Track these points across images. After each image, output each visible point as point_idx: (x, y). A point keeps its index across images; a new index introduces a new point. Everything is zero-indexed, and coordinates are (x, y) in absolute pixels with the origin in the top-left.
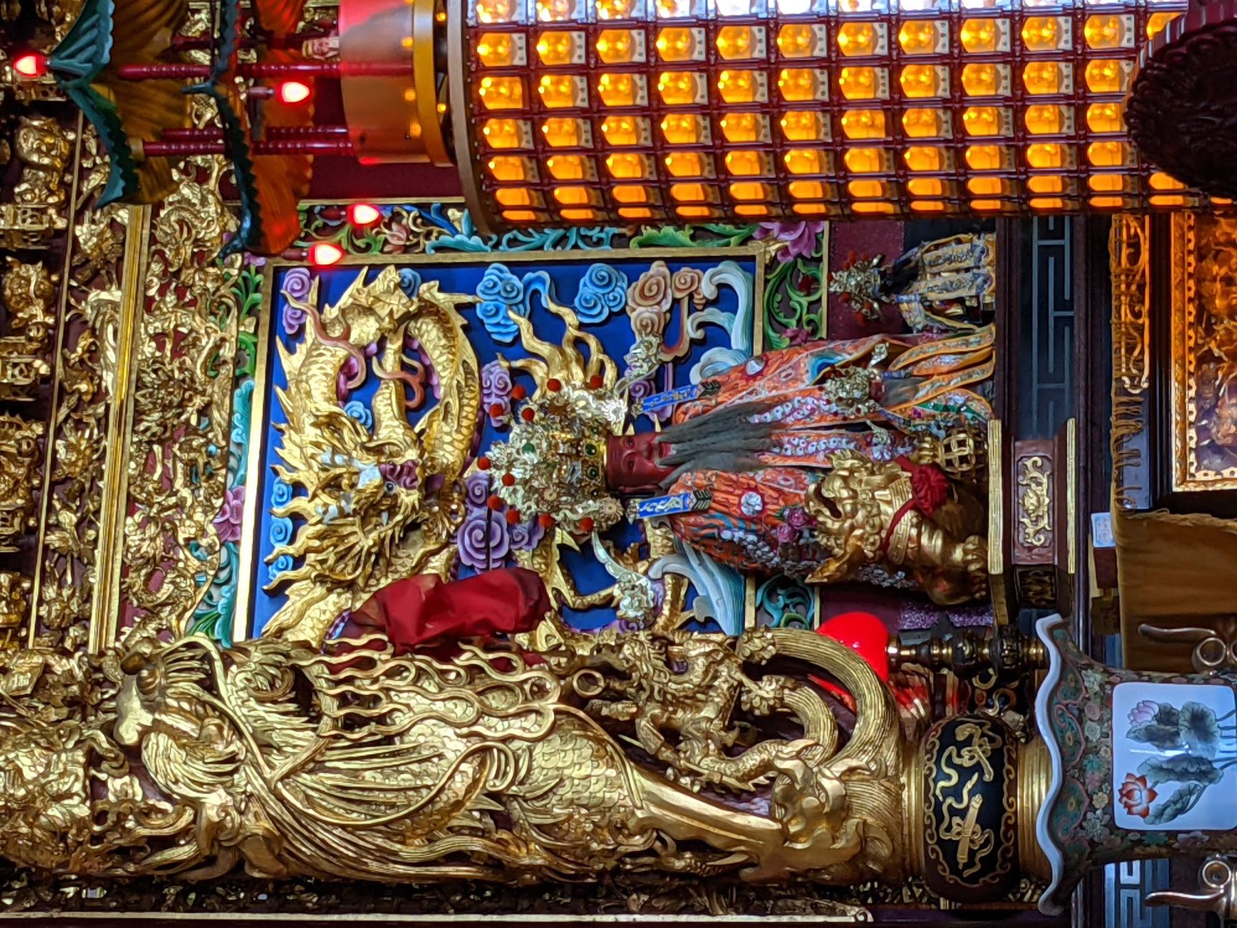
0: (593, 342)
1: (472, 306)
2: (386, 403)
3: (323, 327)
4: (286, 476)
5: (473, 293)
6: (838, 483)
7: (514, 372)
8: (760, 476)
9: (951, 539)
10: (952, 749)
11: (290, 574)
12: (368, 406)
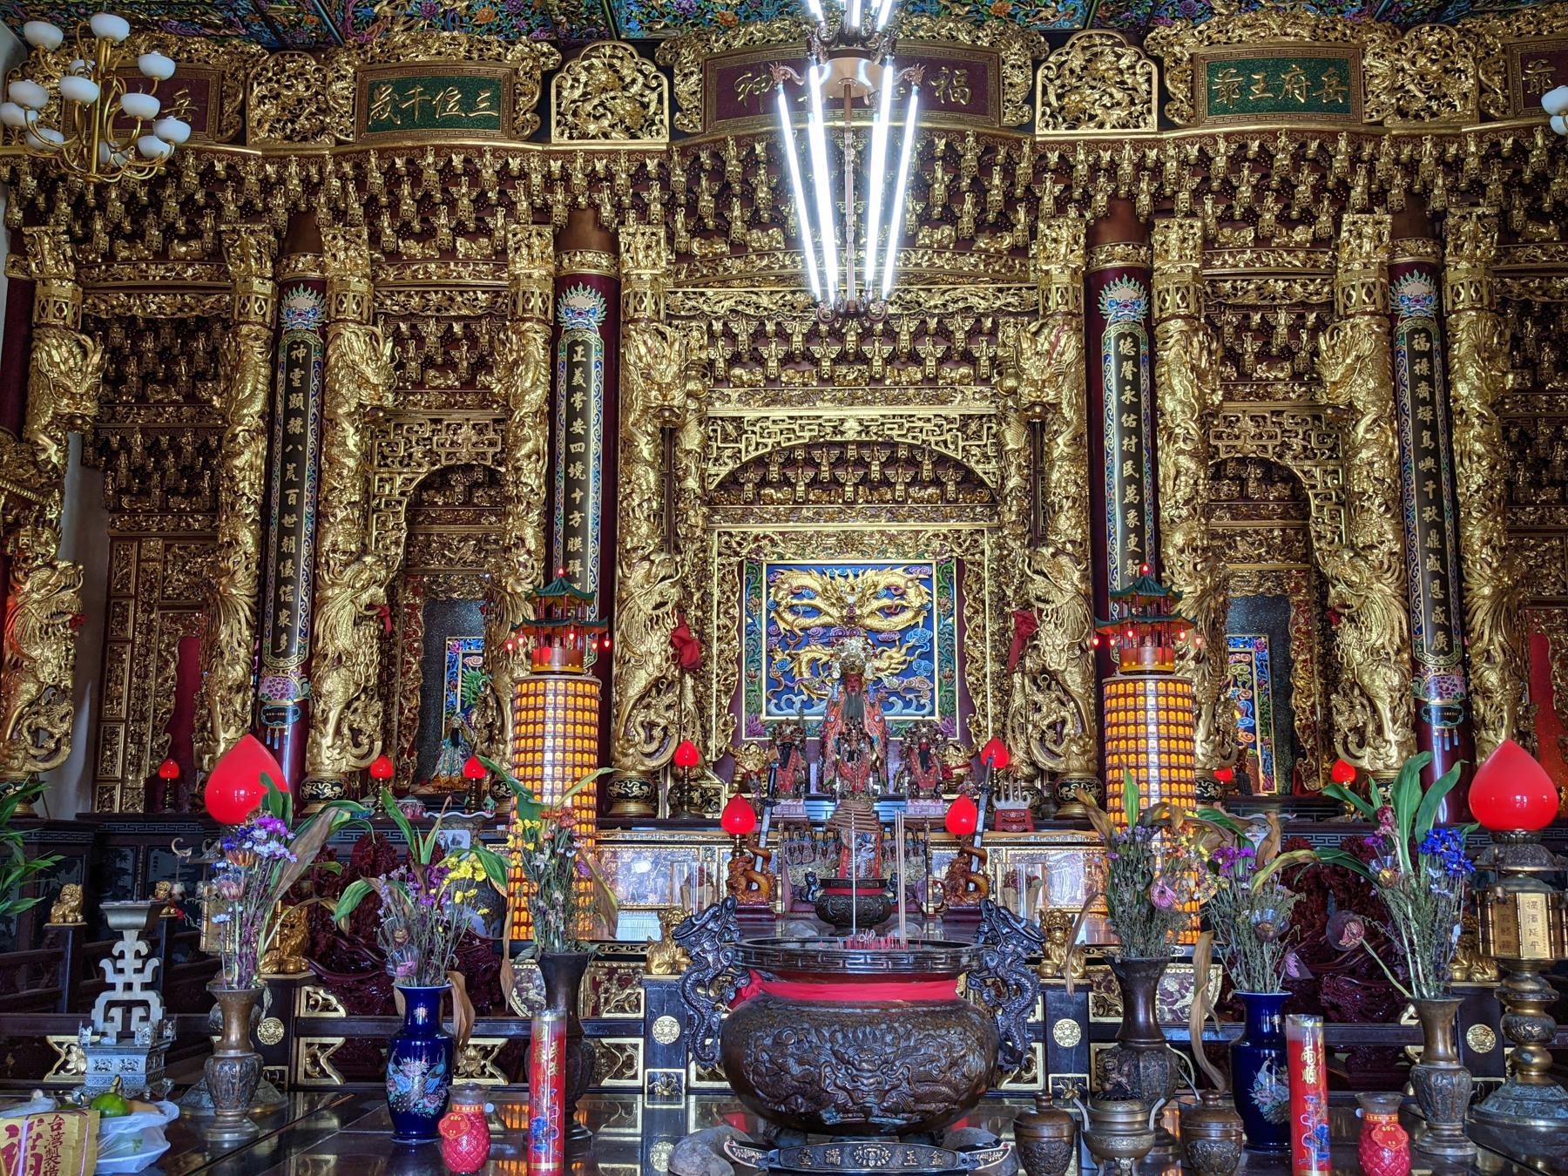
2: (886, 602)
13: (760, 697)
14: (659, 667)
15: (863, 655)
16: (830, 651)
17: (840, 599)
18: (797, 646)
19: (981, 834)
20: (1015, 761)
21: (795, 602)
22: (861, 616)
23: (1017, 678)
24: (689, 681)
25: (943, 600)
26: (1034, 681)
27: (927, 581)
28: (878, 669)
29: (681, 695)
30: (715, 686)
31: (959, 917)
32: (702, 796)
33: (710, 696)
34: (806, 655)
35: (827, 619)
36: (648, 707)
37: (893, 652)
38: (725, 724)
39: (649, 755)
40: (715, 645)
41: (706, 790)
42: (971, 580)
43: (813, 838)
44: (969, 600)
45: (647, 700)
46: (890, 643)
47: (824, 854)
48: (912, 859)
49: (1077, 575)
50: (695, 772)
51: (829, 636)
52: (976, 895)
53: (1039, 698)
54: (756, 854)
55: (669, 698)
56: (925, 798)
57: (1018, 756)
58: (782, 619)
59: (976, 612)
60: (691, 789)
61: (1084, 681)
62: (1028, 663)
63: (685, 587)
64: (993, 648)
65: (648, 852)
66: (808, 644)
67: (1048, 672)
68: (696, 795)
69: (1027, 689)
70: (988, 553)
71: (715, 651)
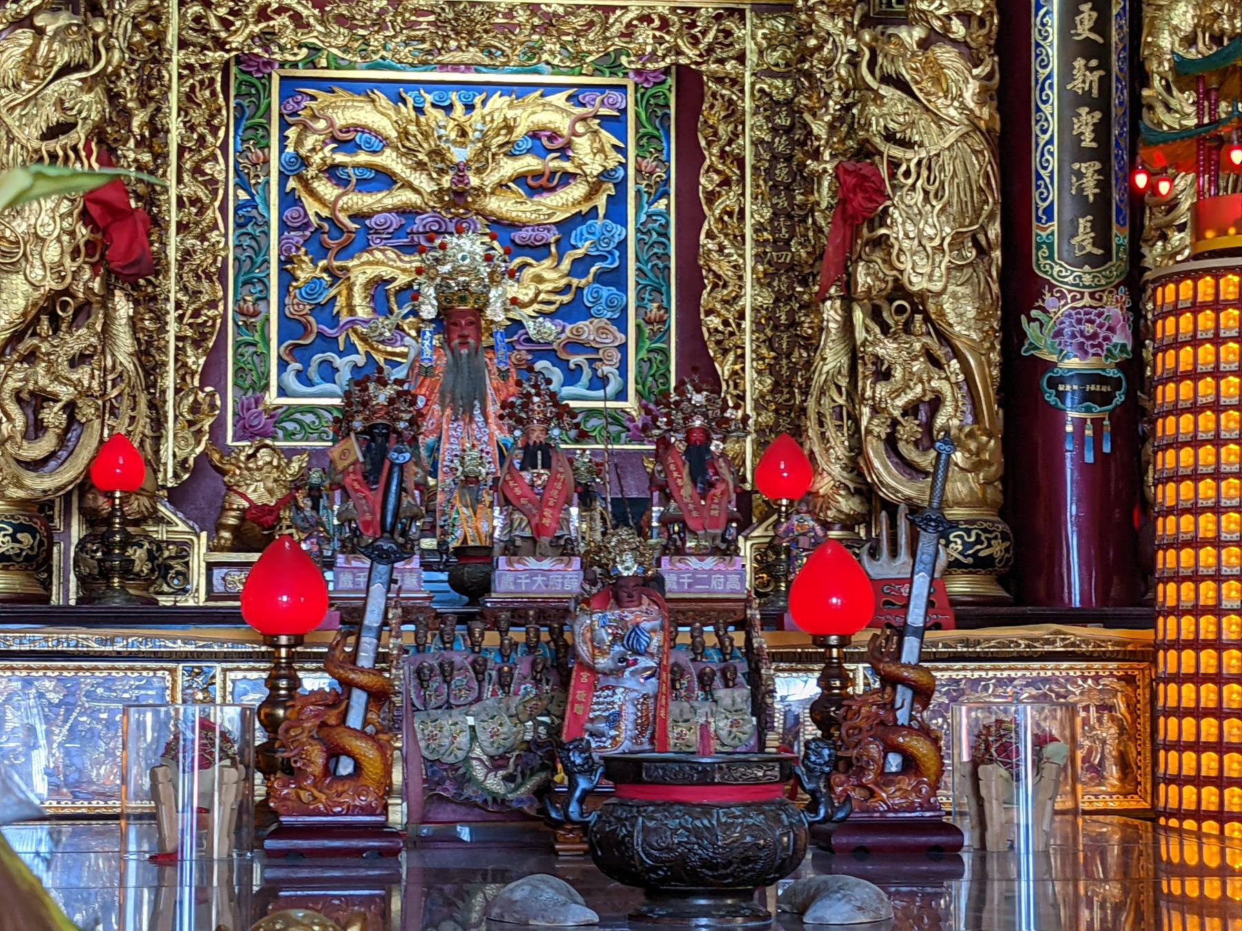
0: (566, 298)
1: (597, 217)
2: (530, 163)
3: (583, 119)
4: (478, 100)
5: (605, 217)
6: (268, 459)
7: (548, 245)
8: (436, 407)
9: (234, 530)
10: (10, 530)
11: (410, 106)
12: (528, 151)
13: (265, 357)
14: (57, 270)
15: (484, 271)
16: (414, 261)
17: (436, 153)
18: (345, 251)
19: (919, 633)
20: (823, 485)
21: (340, 158)
22: (480, 190)
23: (831, 312)
24: (123, 307)
25: (649, 163)
26: (875, 314)
27: (614, 123)
28: (514, 301)
29: (106, 334)
30: (172, 328)
31: (870, 840)
32: (151, 557)
33: (163, 350)
34: (362, 270)
35: (407, 197)
36: (31, 357)
37: (544, 268)
38: (195, 408)
39: (36, 465)
40: (173, 238)
41: (159, 545)
42: (713, 114)
43: (474, 646)
44: (711, 156)
45: (29, 342)
46: (539, 250)
47: (504, 683)
48: (721, 693)
49: (971, 90)
50: (137, 505)
51: (413, 234)
52: (907, 783)
53: (887, 349)
54: (348, 685)
55: (80, 339)
56: (701, 554)
57: (830, 474)
58: (312, 193)
59: (726, 182)
60: (128, 541)
61: (982, 316)
62: (863, 279)
63: (113, 97)
64: (758, 258)
65: (48, 681)
66: (366, 248)
67: (908, 296)
68: (138, 555)
69: (860, 335)
70: (752, 58)
71: (173, 254)
